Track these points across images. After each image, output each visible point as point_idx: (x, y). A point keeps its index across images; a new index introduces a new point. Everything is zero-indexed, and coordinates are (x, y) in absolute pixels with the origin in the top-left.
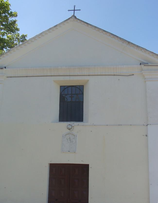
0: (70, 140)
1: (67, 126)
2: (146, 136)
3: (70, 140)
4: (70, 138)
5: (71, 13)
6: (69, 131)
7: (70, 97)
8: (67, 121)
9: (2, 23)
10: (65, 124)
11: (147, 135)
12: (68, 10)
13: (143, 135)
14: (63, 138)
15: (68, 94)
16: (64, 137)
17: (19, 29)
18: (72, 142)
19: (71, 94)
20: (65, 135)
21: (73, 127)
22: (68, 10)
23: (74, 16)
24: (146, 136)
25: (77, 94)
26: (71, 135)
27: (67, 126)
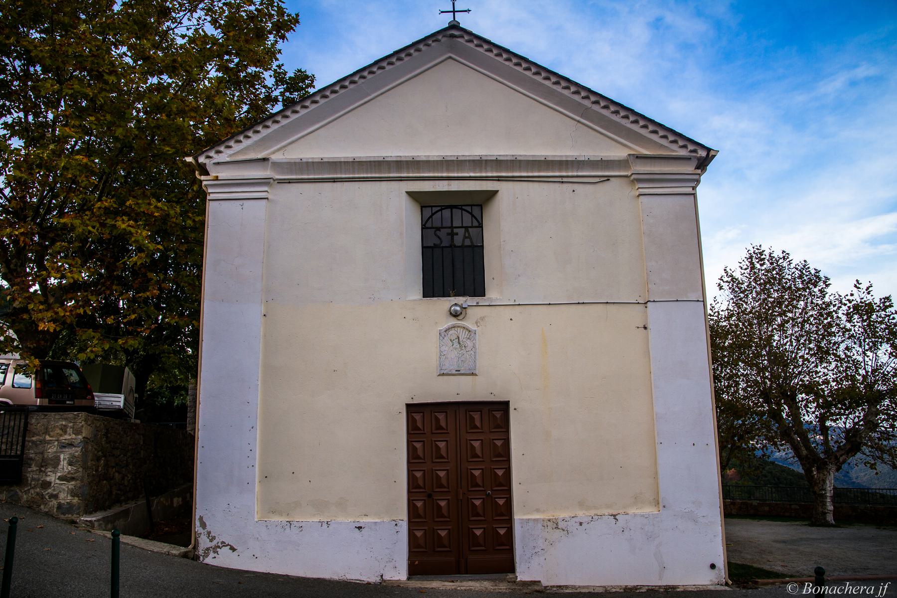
0: (459, 343)
1: (451, 308)
2: (645, 328)
3: (459, 343)
4: (459, 338)
5: (449, 18)
6: (453, 321)
7: (448, 234)
8: (445, 294)
9: (209, 59)
10: (445, 304)
11: (646, 326)
12: (470, 11)
13: (638, 328)
14: (441, 338)
15: (443, 228)
16: (443, 336)
17: (299, 71)
18: (464, 348)
19: (449, 228)
20: (446, 331)
21: (464, 310)
22: (470, 11)
23: (454, 26)
24: (645, 328)
25: (465, 227)
26: (462, 330)
27: (451, 308)
